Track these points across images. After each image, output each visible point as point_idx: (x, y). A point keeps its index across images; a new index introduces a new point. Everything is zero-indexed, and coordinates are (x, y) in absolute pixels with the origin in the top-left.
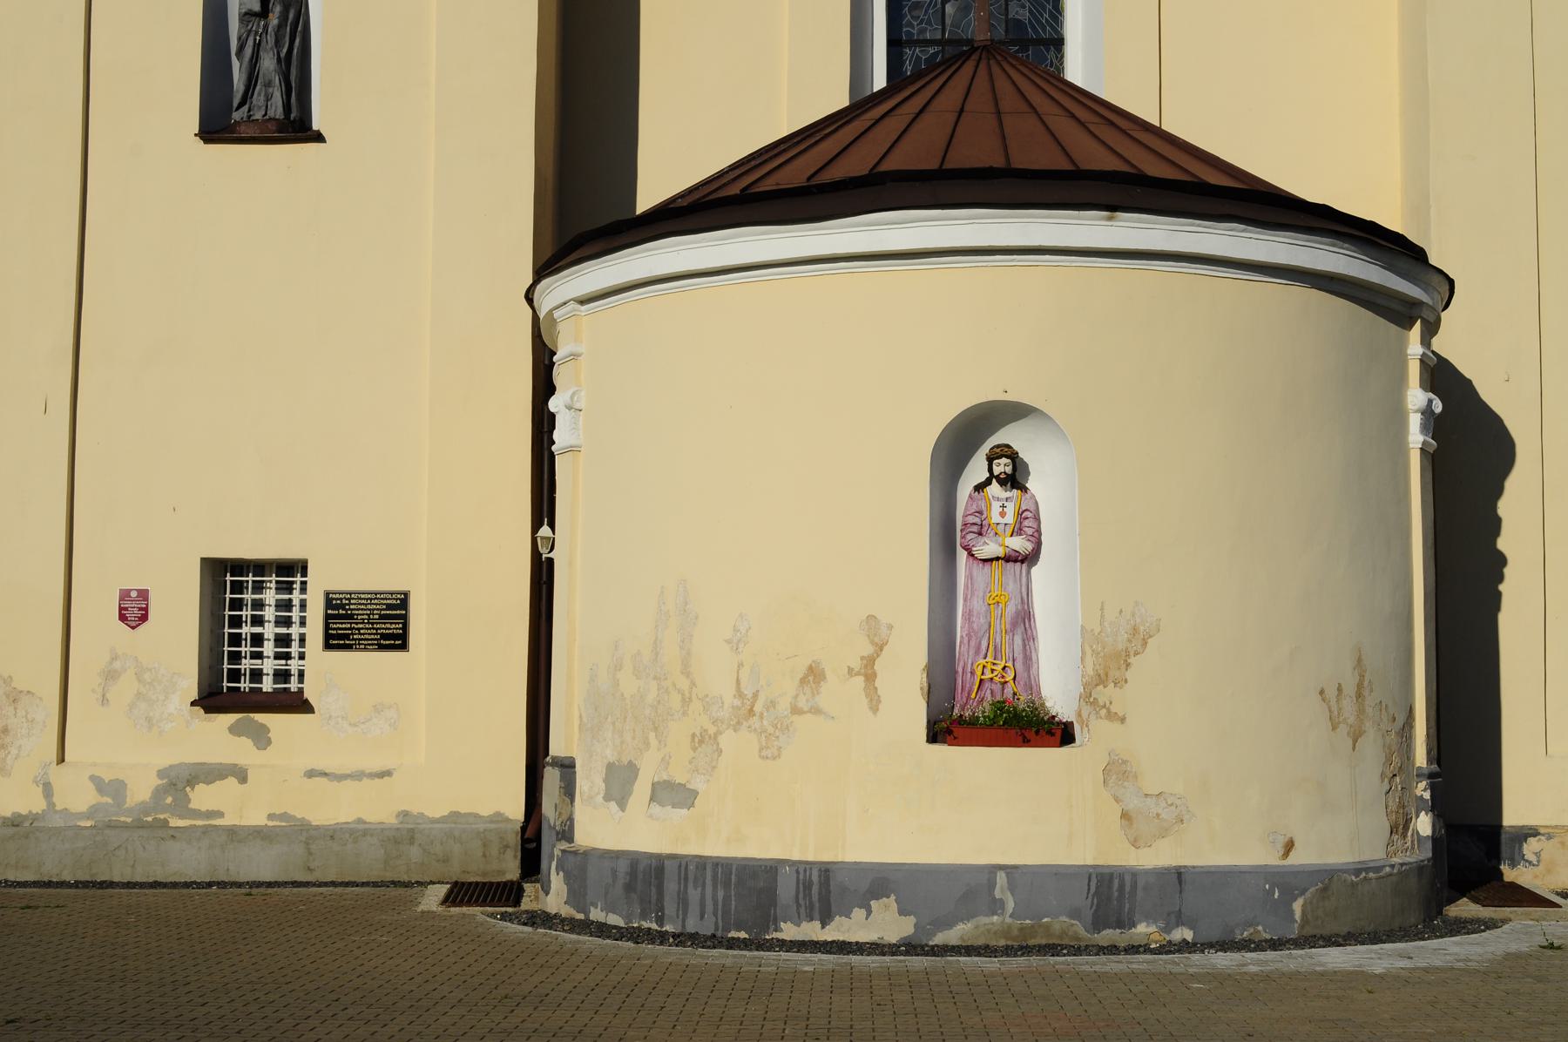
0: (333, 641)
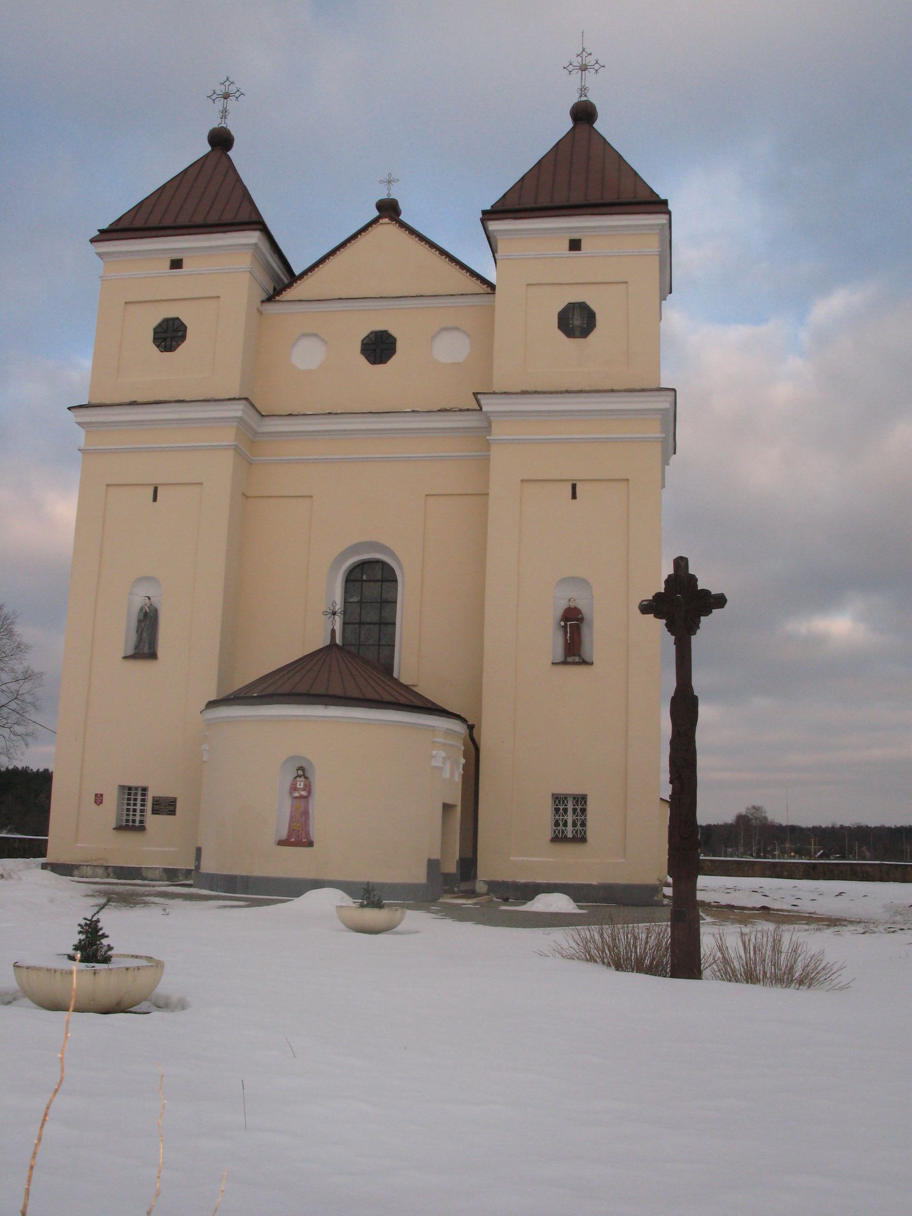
0: (155, 812)
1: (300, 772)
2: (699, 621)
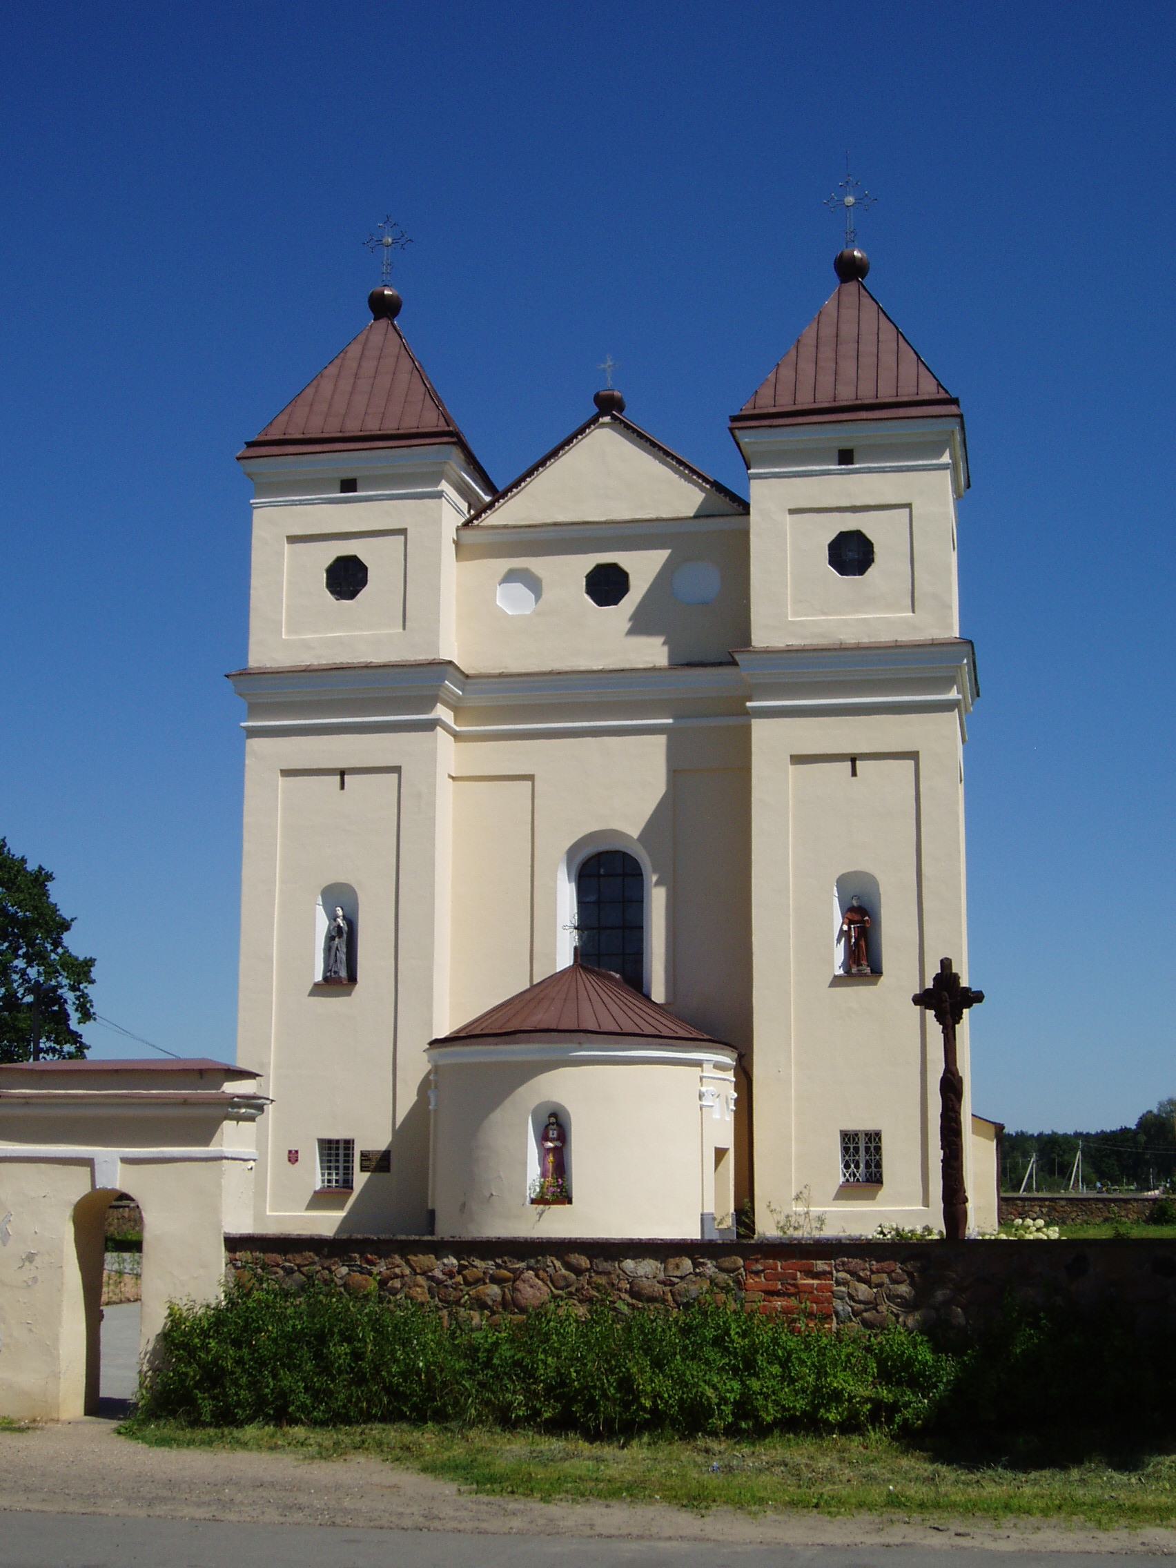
1: (553, 1120)
2: (962, 1013)
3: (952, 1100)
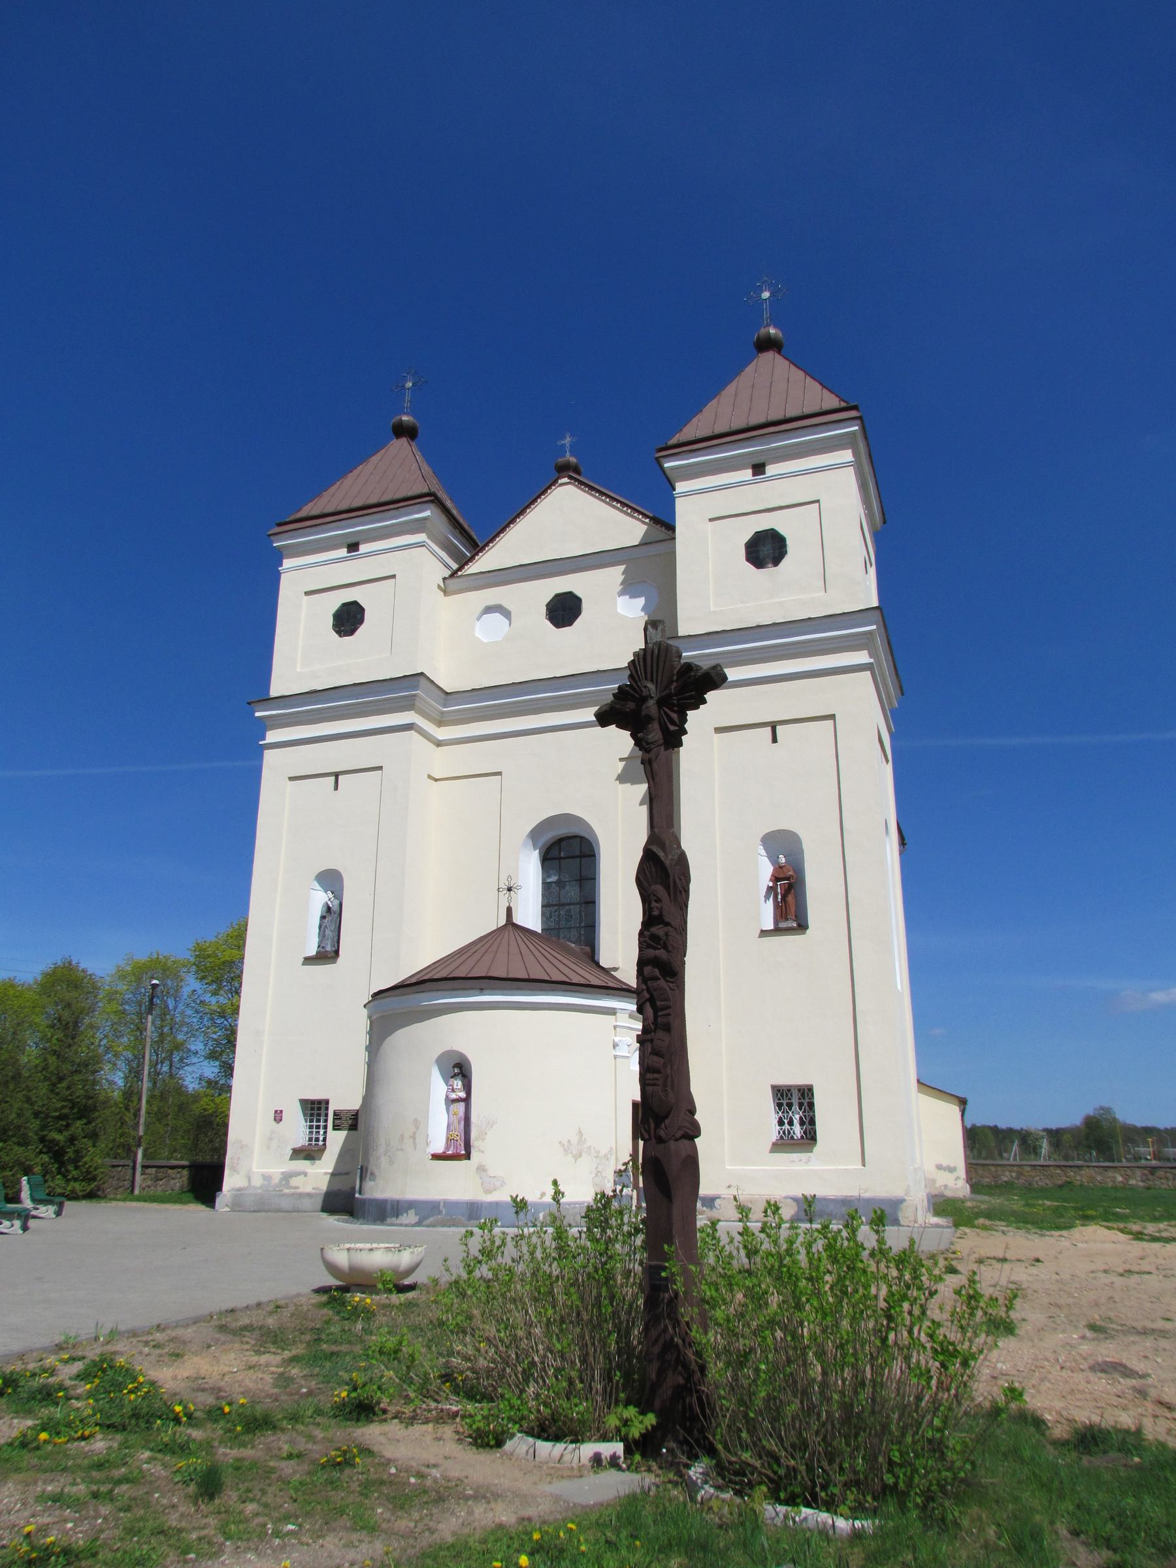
3: (658, 900)
